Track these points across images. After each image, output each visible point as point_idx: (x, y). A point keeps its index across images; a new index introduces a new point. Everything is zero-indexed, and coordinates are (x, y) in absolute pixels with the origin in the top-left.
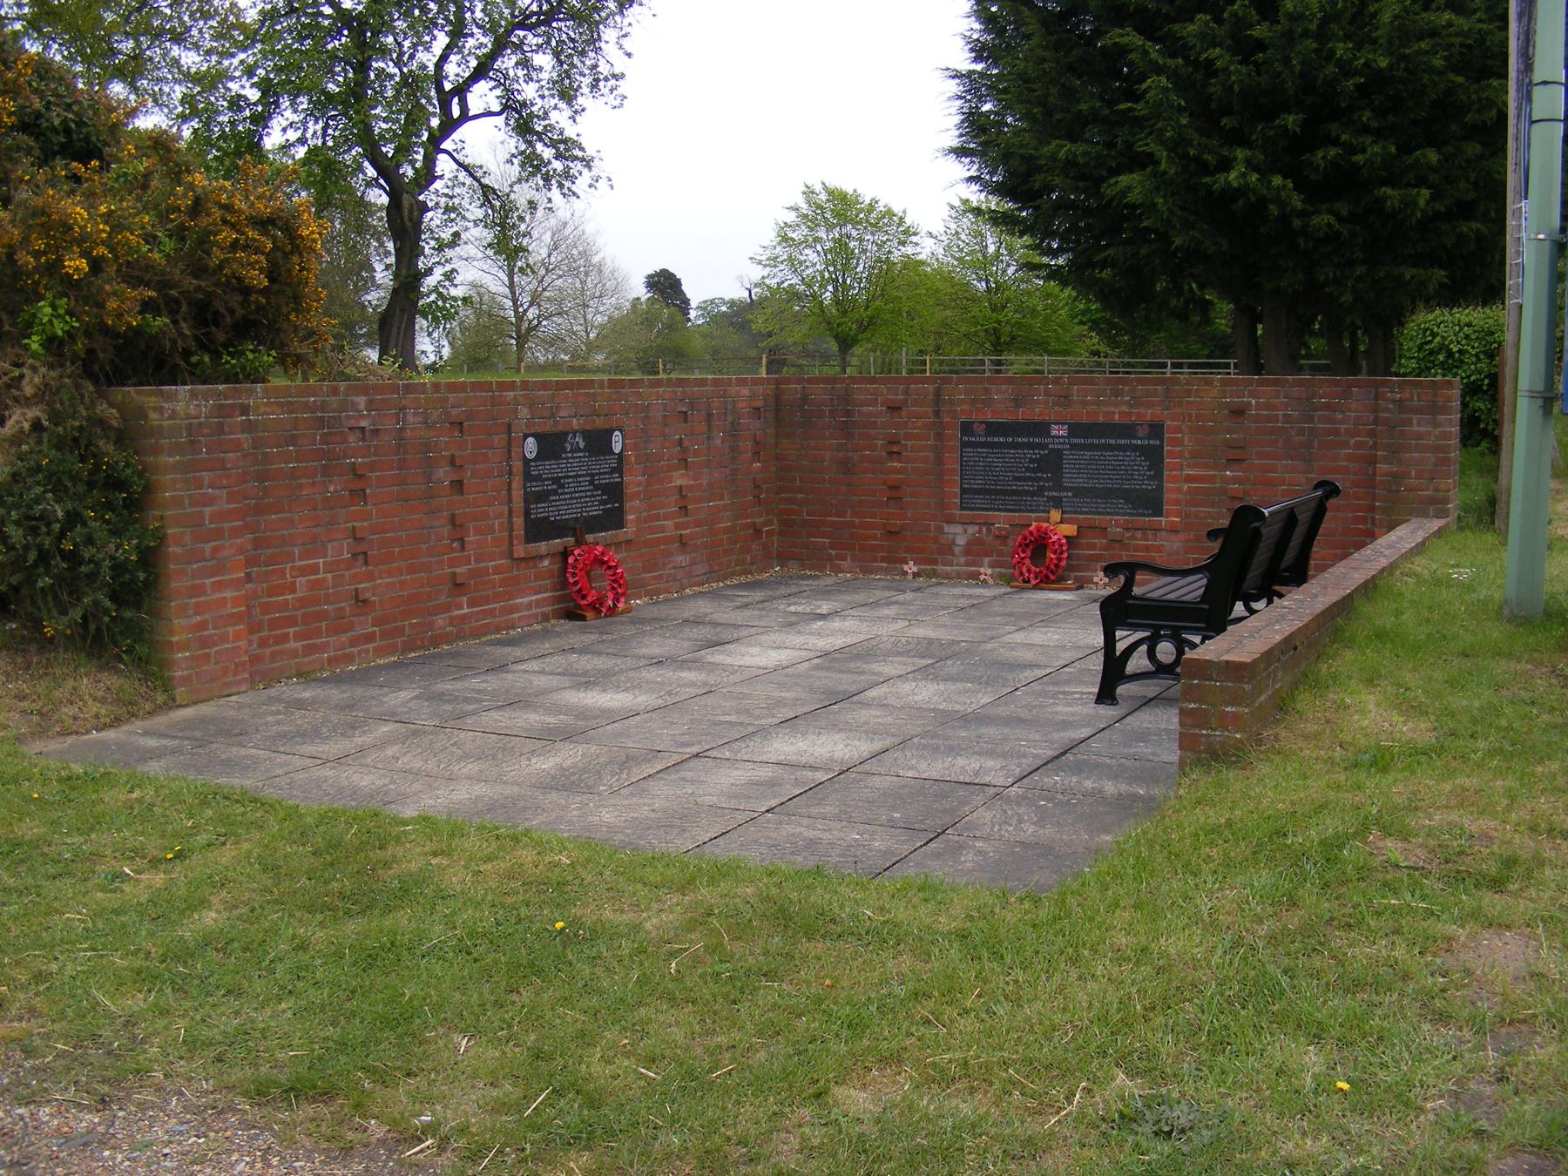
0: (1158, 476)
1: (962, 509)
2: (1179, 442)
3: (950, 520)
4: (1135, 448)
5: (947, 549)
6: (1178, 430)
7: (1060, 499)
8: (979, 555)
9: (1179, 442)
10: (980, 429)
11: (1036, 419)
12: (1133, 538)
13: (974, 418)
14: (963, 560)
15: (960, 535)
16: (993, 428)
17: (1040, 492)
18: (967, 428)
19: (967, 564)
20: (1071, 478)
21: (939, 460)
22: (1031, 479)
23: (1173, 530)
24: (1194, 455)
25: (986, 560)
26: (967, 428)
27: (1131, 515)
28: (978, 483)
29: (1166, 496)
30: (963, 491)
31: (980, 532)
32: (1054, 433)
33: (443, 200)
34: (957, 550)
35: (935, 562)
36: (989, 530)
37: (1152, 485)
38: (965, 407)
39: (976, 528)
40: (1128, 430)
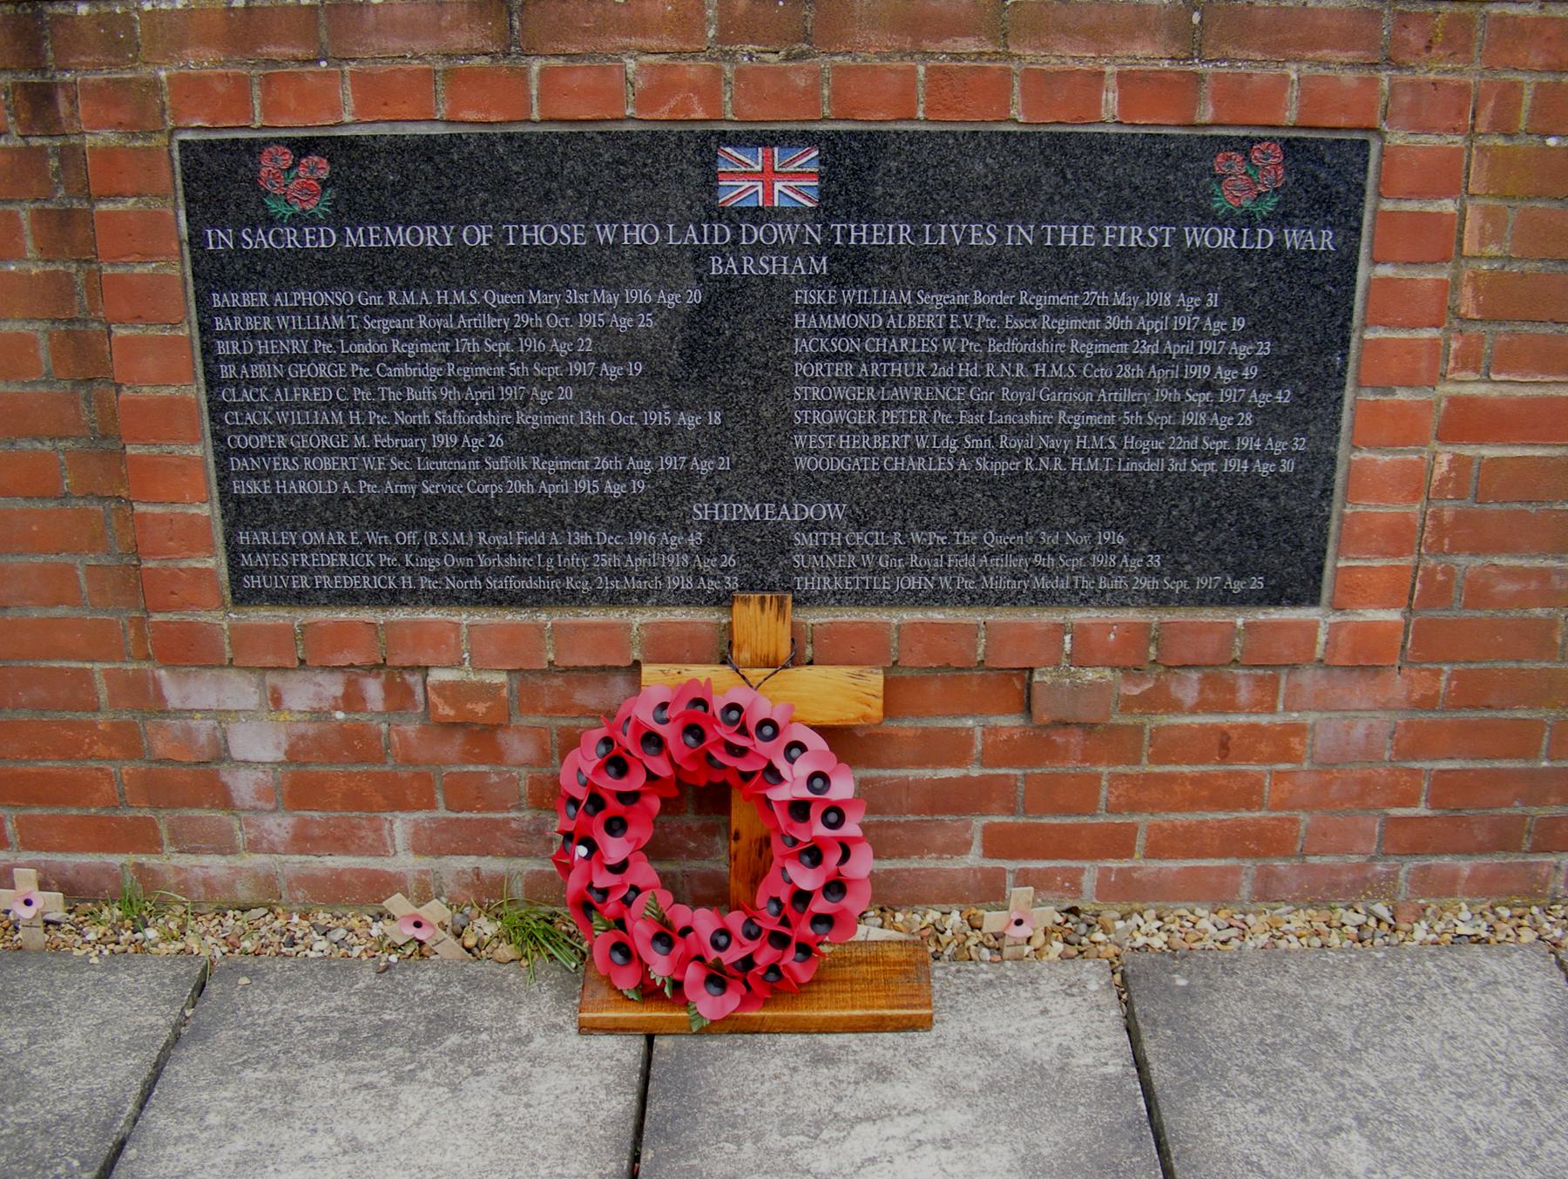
0: (1321, 392)
1: (242, 597)
2: (1440, 241)
3: (189, 651)
4: (1196, 271)
5: (202, 780)
6: (1445, 176)
7: (778, 541)
8: (355, 801)
9: (1440, 241)
10: (296, 188)
11: (631, 115)
12: (1159, 700)
13: (257, 122)
14: (279, 825)
15: (247, 716)
16: (363, 174)
17: (666, 502)
18: (219, 179)
19: (303, 841)
20: (831, 424)
21: (86, 359)
22: (611, 441)
23: (1364, 659)
24: (1502, 302)
25: (400, 825)
26: (219, 179)
27: (1160, 599)
28: (316, 474)
29: (1342, 509)
30: (237, 511)
31: (352, 699)
32: (736, 191)
33: (1503, 1133)
34: (243, 785)
35: (142, 837)
36: (399, 696)
37: (1282, 454)
38: (201, 61)
39: (334, 686)
40: (1162, 173)
